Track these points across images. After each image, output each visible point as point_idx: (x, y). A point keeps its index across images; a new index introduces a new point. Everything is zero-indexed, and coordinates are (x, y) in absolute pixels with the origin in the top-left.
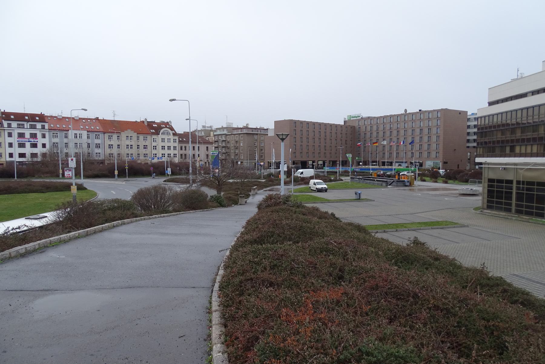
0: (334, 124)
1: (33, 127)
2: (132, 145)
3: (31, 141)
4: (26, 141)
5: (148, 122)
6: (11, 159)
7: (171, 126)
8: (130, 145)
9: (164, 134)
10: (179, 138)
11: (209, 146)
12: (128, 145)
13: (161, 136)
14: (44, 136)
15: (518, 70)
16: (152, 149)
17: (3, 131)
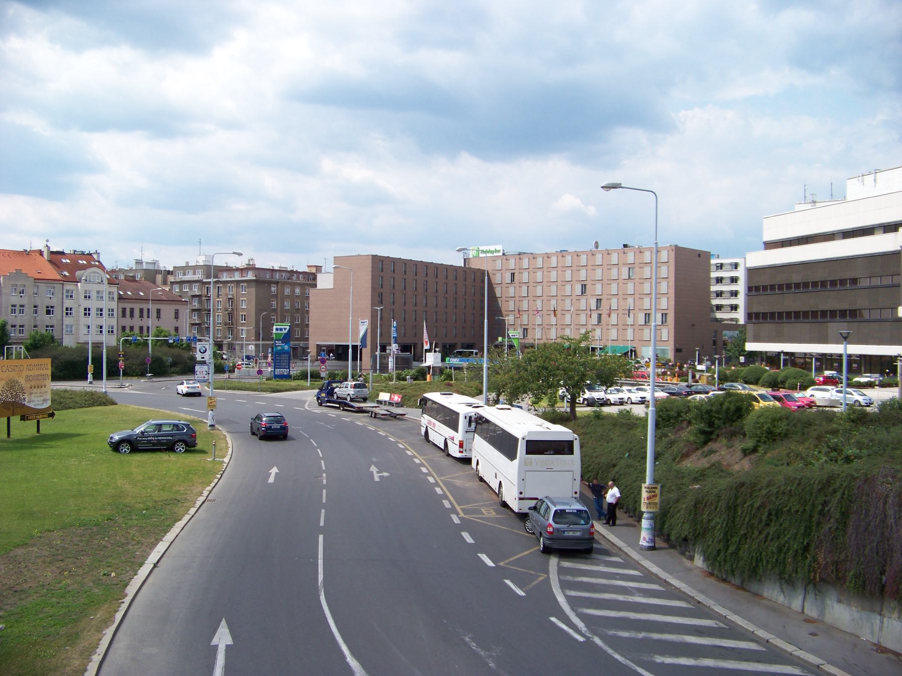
0: (359, 256)
2: (23, 306)
5: (52, 253)
7: (99, 262)
8: (18, 306)
10: (119, 289)
11: (181, 308)
12: (15, 306)
15: (875, 180)
16: (64, 314)
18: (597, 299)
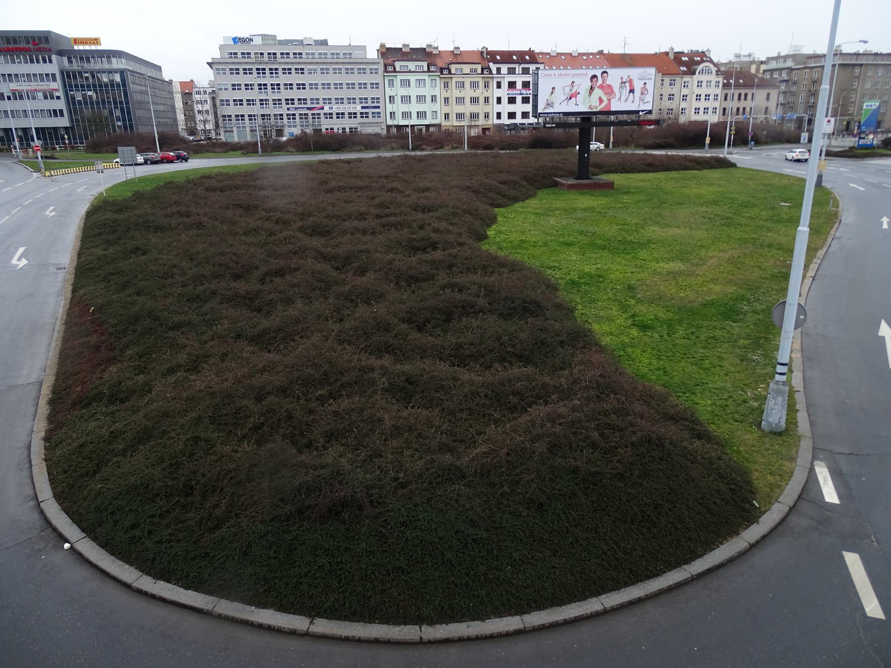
3: (523, 94)
6: (499, 122)
9: (702, 73)
13: (697, 77)
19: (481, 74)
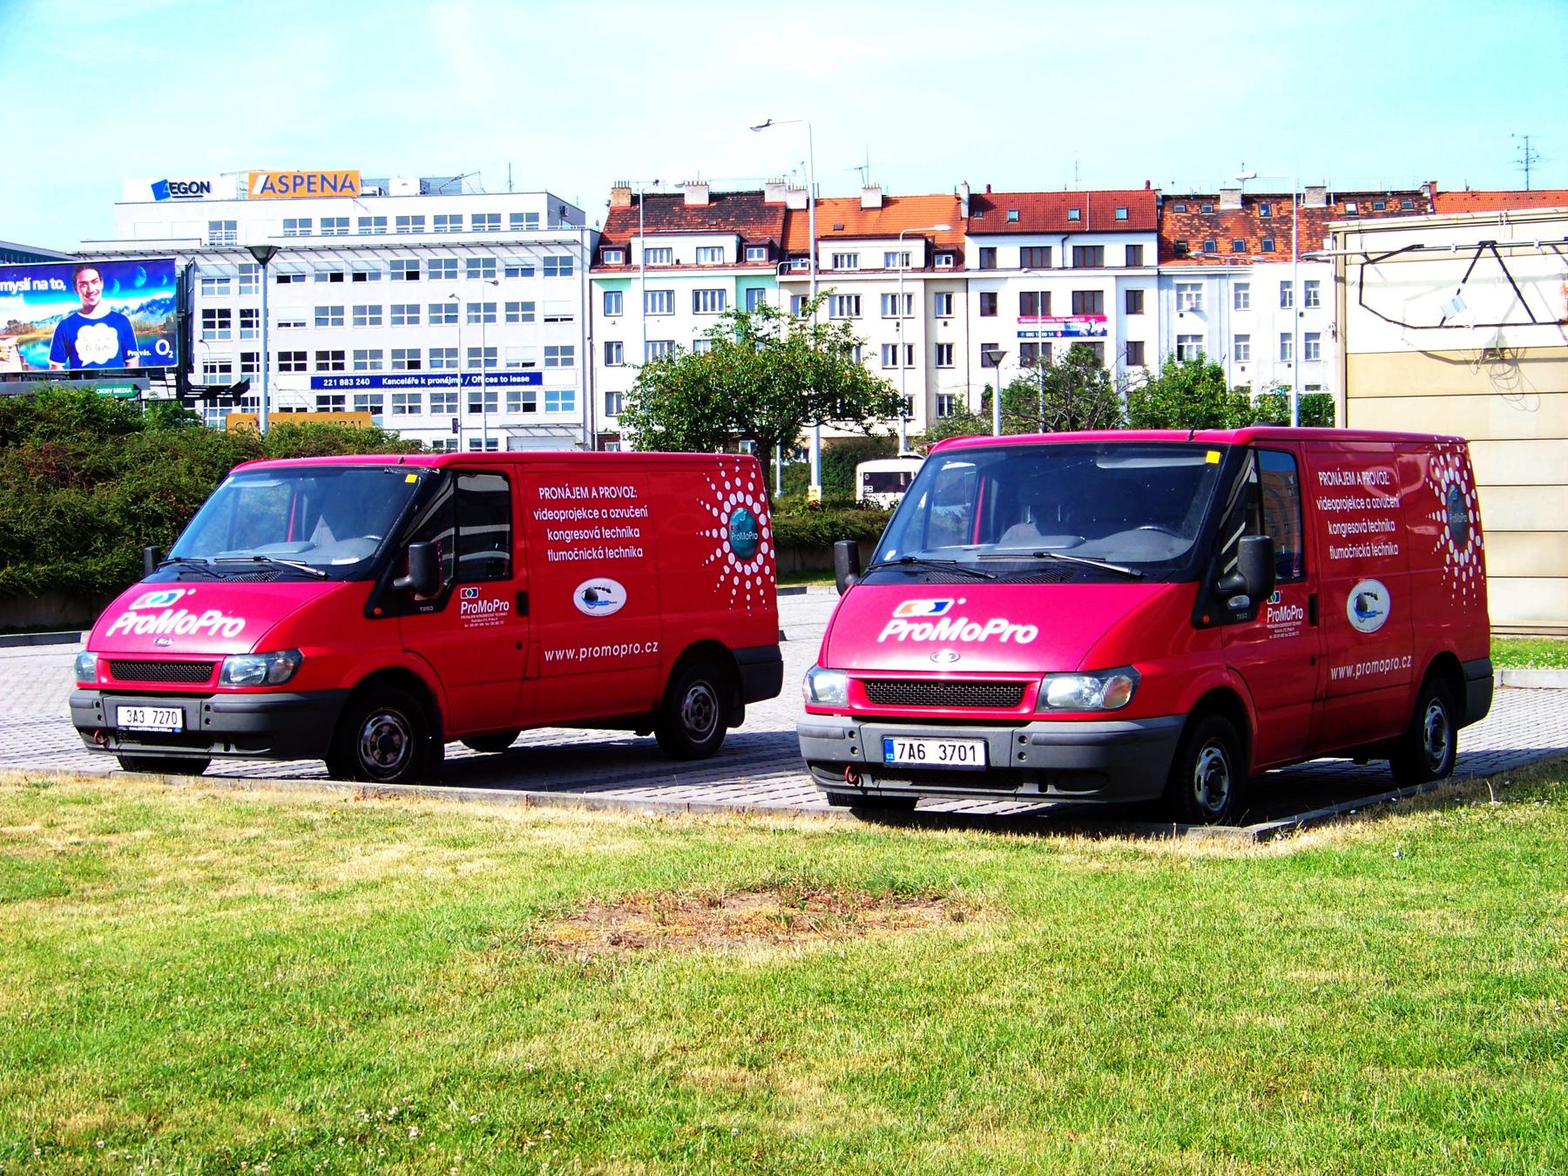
1: (1088, 258)
3: (1077, 334)
4: (1055, 333)
14: (1134, 302)
17: (962, 286)
18: (884, 296)
19: (923, 270)
